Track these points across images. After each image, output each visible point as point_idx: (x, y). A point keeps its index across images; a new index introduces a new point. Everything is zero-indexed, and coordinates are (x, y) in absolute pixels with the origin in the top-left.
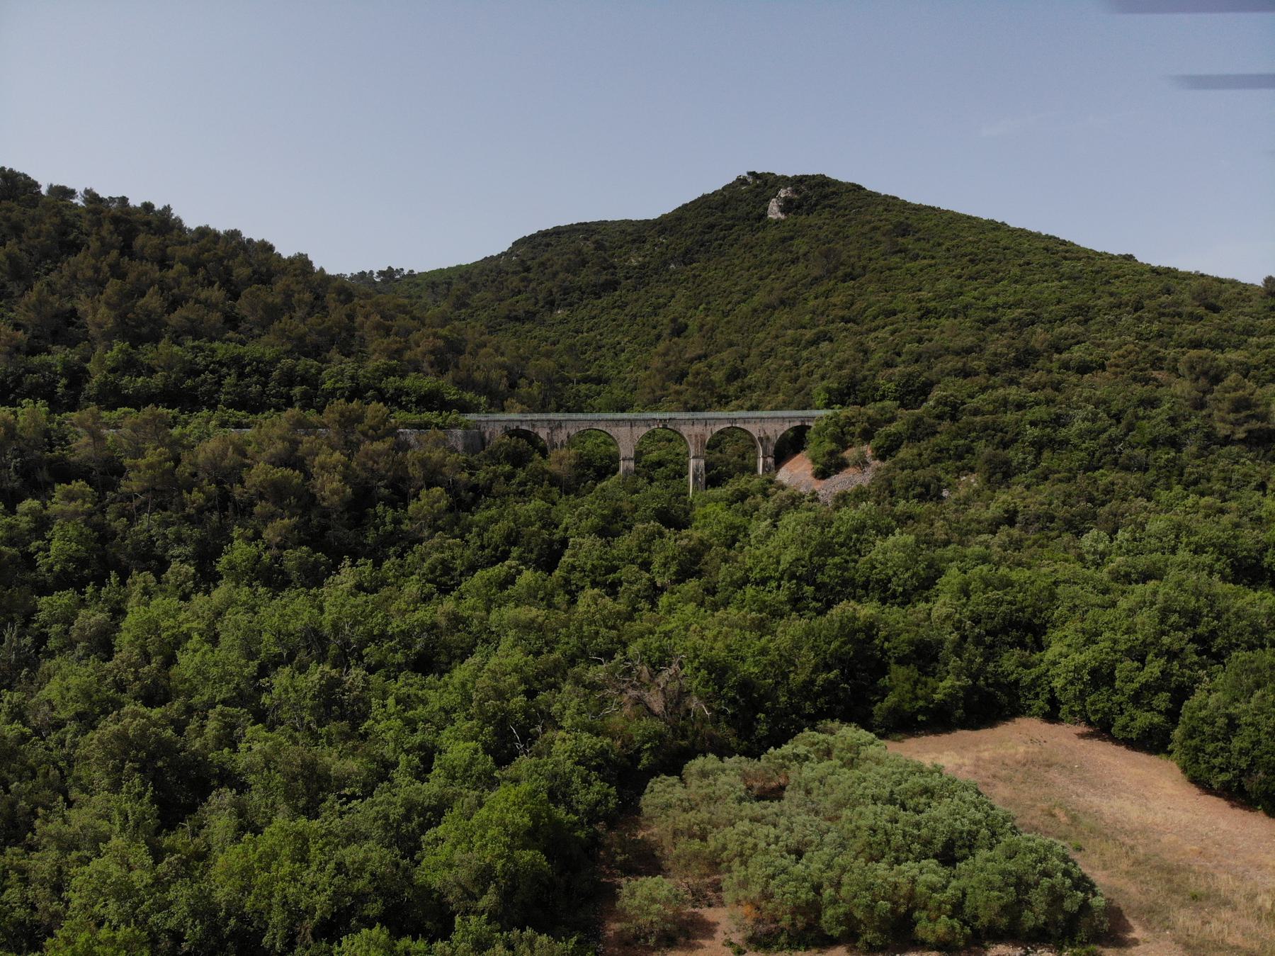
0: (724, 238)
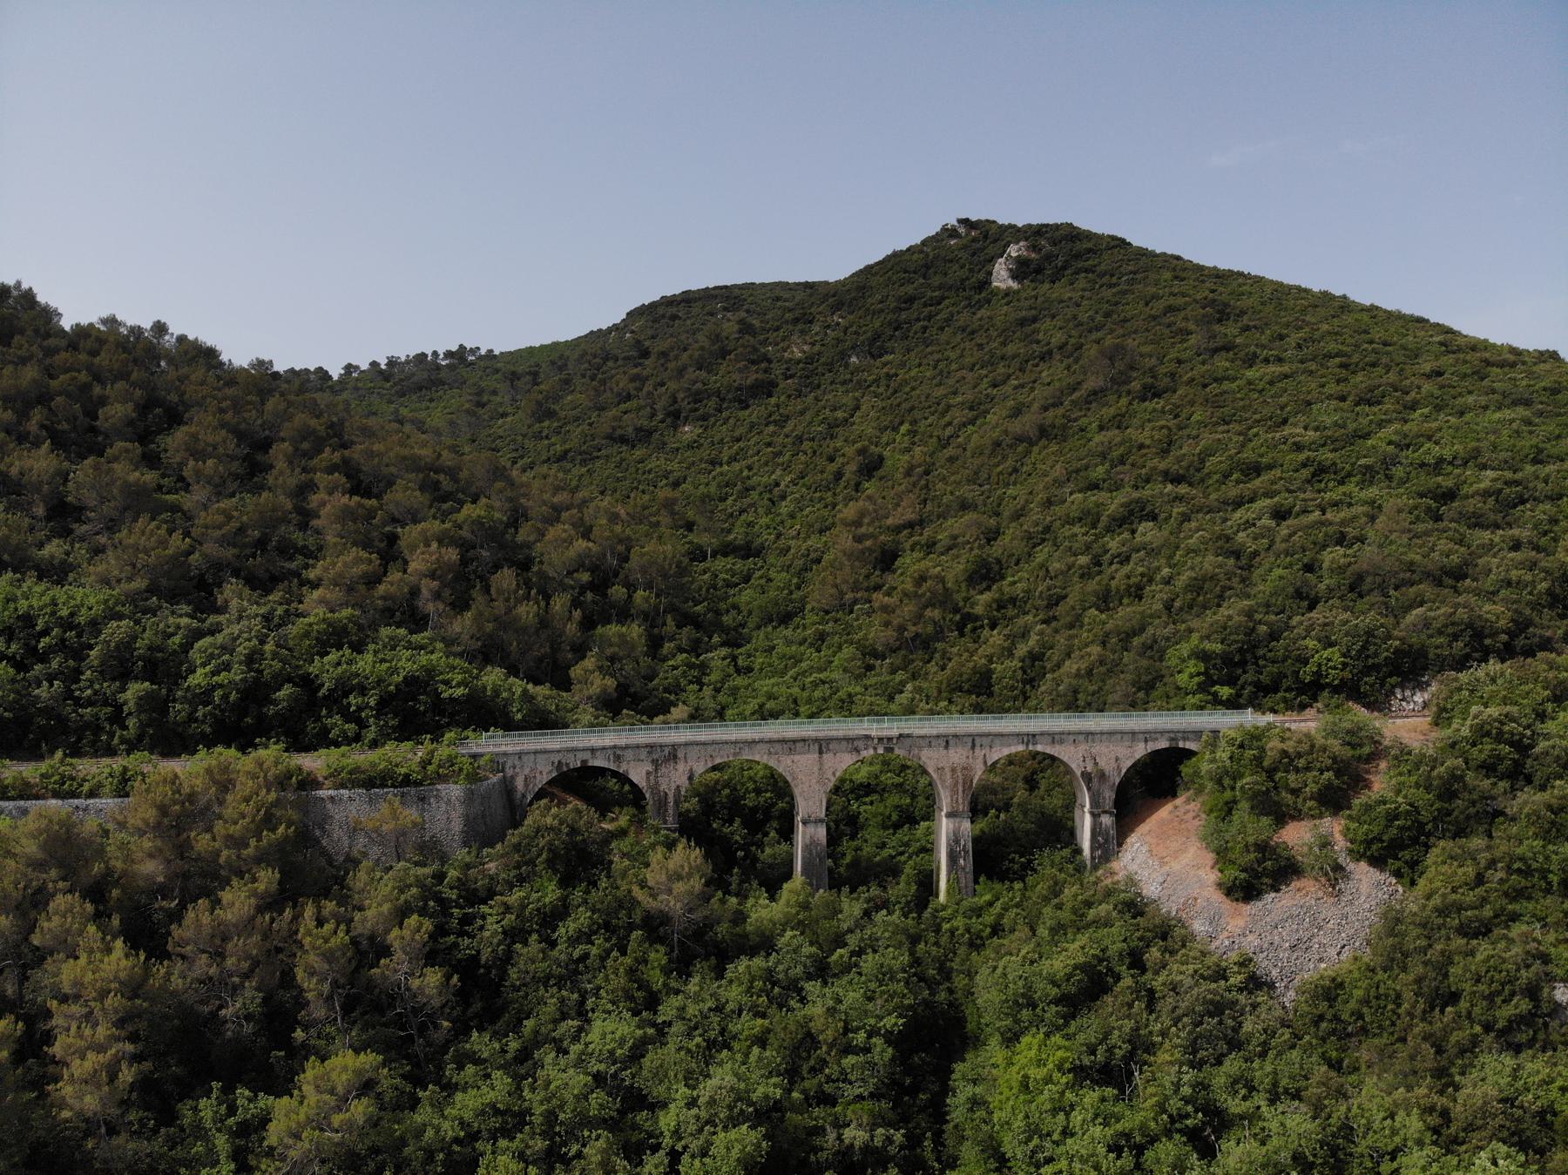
0: (929, 317)
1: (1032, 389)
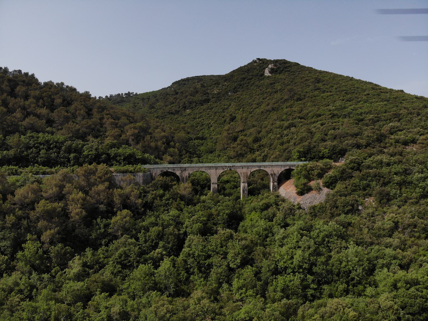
0: (249, 83)
1: (272, 100)
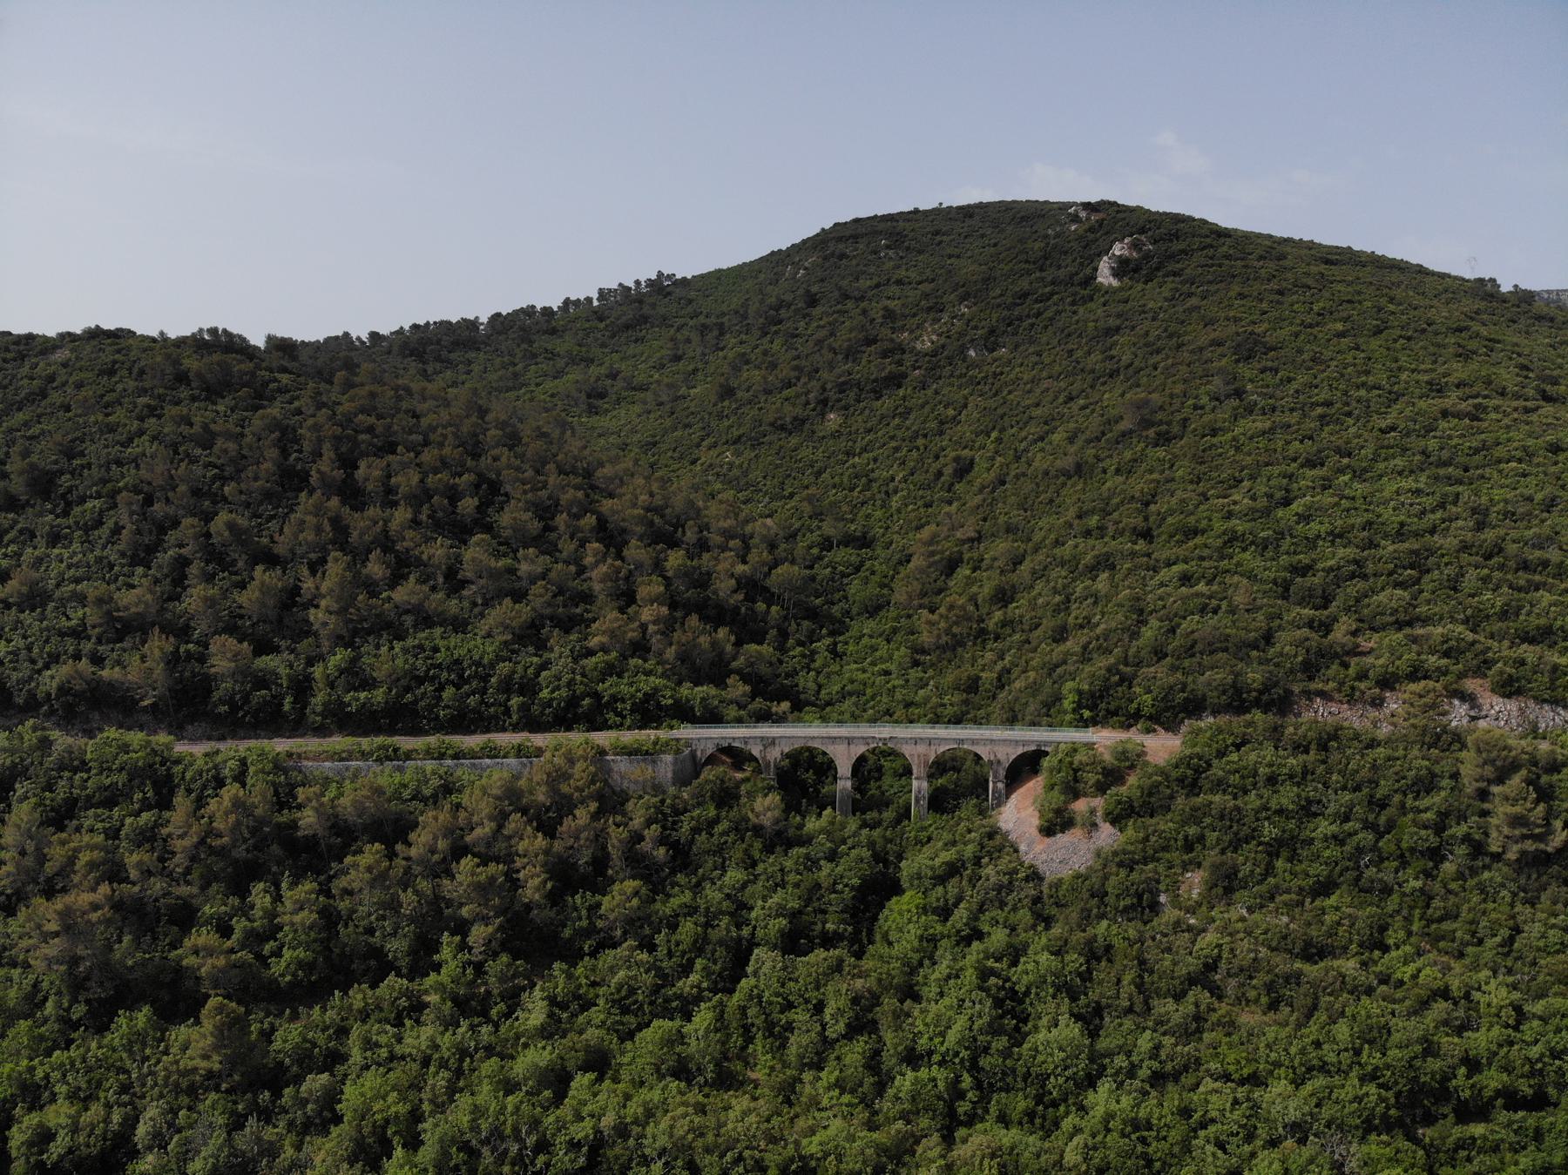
0: (1039, 314)
